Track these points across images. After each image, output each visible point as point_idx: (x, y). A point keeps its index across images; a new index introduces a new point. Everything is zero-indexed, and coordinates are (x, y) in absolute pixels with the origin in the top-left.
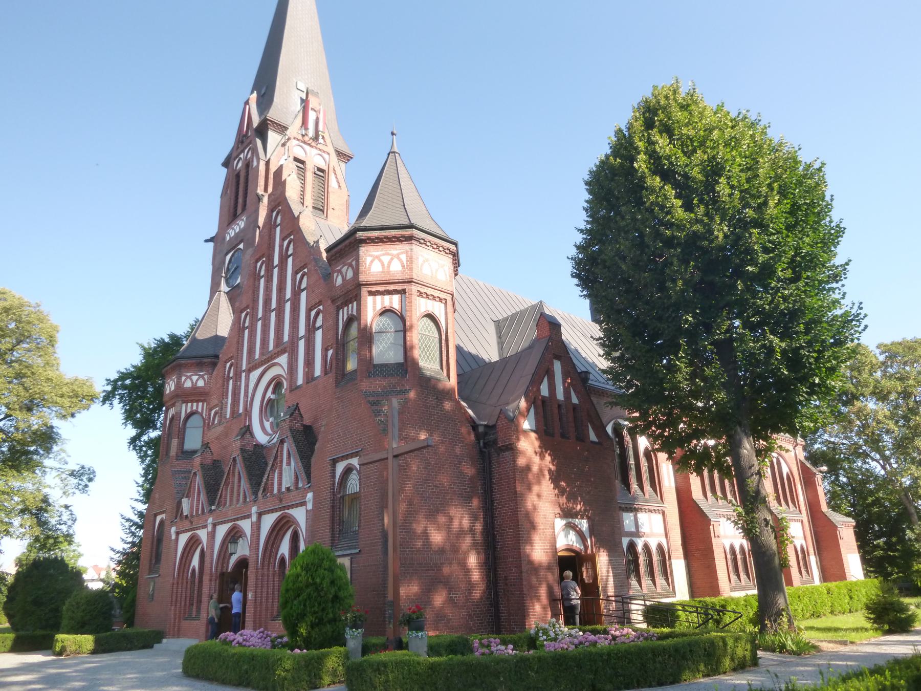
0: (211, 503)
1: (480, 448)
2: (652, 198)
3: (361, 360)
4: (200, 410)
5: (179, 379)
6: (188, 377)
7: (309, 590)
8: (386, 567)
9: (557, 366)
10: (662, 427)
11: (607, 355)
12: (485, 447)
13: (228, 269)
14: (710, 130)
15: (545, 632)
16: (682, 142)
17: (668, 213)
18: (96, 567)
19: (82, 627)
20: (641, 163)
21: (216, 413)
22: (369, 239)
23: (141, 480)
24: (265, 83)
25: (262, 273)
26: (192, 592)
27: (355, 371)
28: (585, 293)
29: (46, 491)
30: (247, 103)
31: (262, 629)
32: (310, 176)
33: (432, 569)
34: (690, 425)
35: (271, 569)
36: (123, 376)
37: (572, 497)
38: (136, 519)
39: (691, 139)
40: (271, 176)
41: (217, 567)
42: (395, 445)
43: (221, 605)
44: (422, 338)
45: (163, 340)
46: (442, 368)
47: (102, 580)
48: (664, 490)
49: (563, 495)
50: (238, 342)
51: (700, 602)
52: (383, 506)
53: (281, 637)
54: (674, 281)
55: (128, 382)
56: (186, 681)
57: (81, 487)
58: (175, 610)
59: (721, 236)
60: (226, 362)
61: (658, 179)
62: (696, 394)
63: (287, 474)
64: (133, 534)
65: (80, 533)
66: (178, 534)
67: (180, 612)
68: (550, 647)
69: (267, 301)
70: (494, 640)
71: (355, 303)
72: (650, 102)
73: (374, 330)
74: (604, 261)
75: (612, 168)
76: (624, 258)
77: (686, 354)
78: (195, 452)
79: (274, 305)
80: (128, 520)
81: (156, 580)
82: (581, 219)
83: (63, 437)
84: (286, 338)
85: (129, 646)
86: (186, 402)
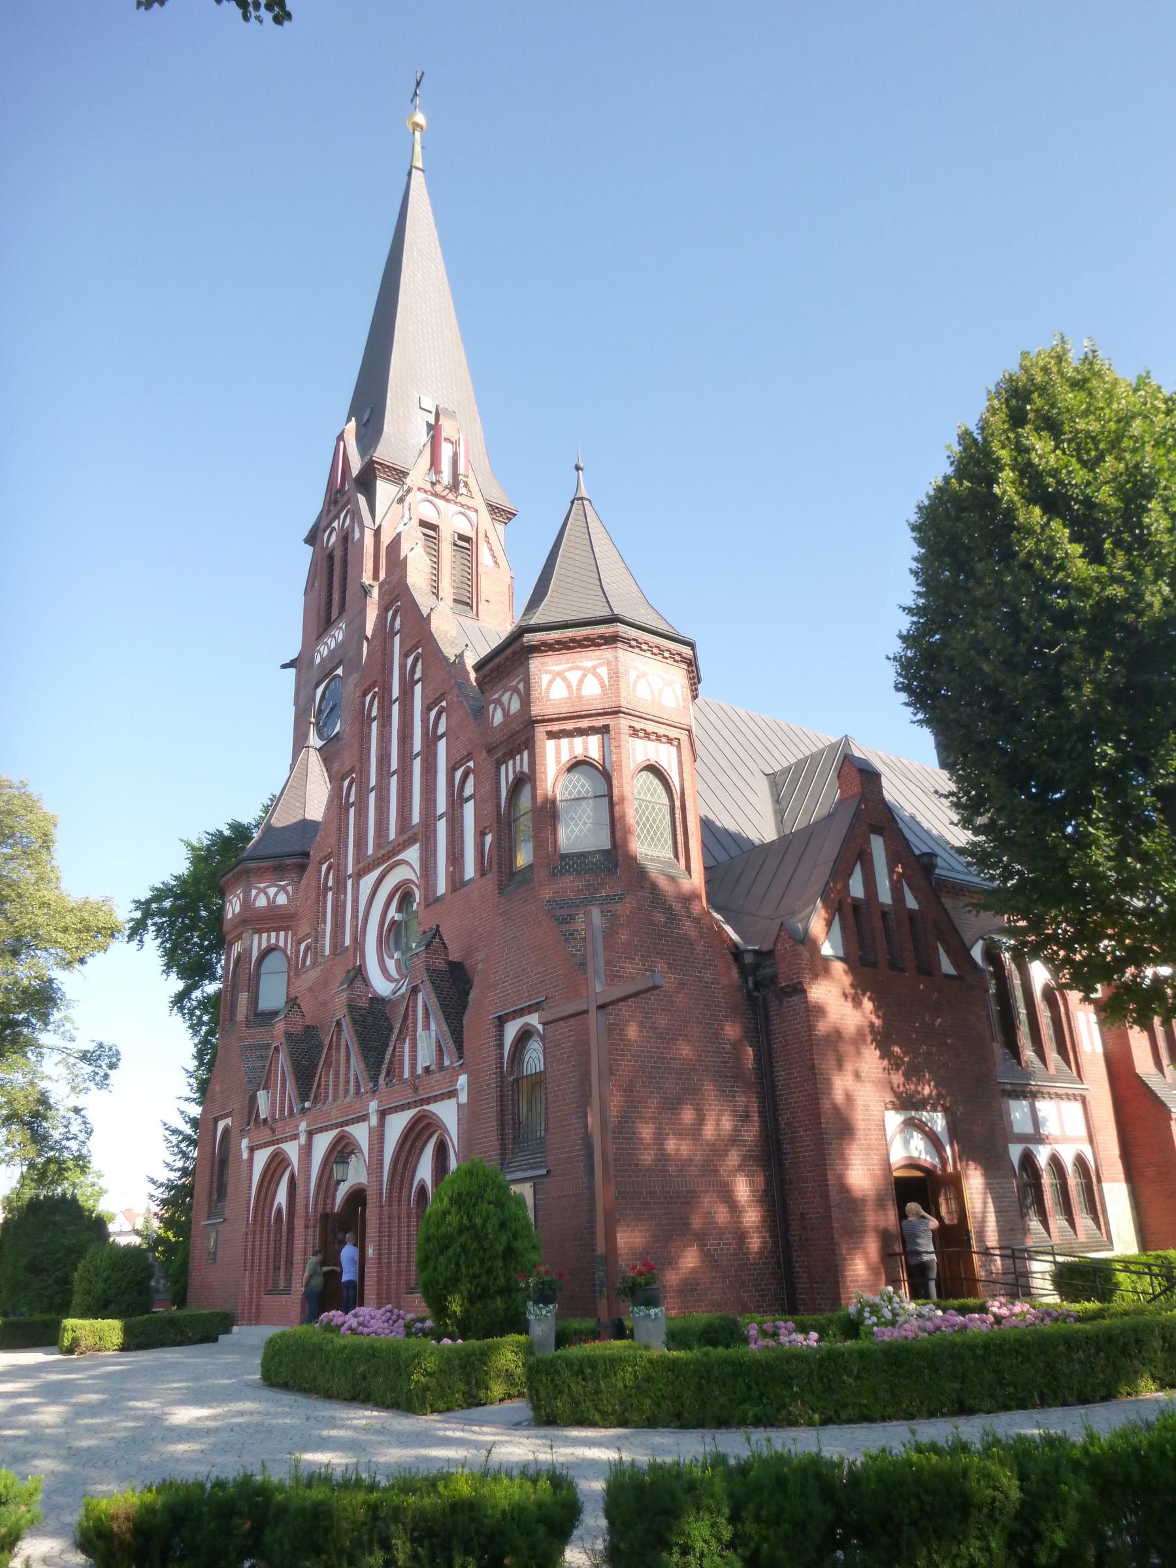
0: (304, 1097)
1: (749, 992)
2: (1029, 544)
3: (539, 847)
4: (281, 944)
5: (247, 893)
6: (260, 890)
7: (463, 1239)
8: (592, 1199)
9: (878, 846)
10: (1067, 944)
11: (966, 823)
12: (756, 989)
13: (320, 711)
14: (1125, 420)
15: (875, 1309)
16: (1078, 445)
17: (1061, 568)
18: (128, 1213)
19: (105, 1307)
20: (1006, 486)
21: (307, 948)
22: (544, 644)
23: (192, 1064)
24: (369, 405)
25: (374, 713)
26: (278, 1247)
27: (530, 867)
28: (920, 716)
29: (43, 1084)
30: (341, 437)
31: (389, 1306)
32: (446, 550)
33: (671, 1203)
34: (1120, 941)
35: (404, 1207)
36: (160, 894)
37: (912, 1073)
38: (187, 1129)
39: (1093, 439)
40: (383, 553)
41: (316, 1205)
42: (599, 988)
43: (325, 1269)
44: (640, 798)
45: (221, 832)
46: (677, 857)
47: (137, 1233)
48: (1083, 1060)
49: (897, 1070)
50: (339, 829)
51: (1158, 1257)
52: (584, 1100)
53: (422, 1320)
54: (1078, 686)
55: (167, 904)
56: (268, 1393)
57: (97, 1078)
58: (251, 1277)
59: (1157, 602)
60: (321, 863)
61: (1037, 511)
62: (1129, 886)
63: (424, 1044)
64: (185, 1155)
65: (99, 1152)
66: (252, 1150)
67: (259, 1281)
68: (888, 1335)
69: (384, 758)
70: (785, 1325)
71: (526, 753)
72: (1017, 380)
73: (558, 798)
74: (951, 660)
75: (956, 498)
76: (985, 653)
77: (1107, 814)
78: (275, 1013)
79: (394, 765)
80: (175, 1132)
81: (220, 1227)
82: (906, 589)
83: (68, 996)
84: (416, 818)
85: (179, 1338)
86: (259, 931)
